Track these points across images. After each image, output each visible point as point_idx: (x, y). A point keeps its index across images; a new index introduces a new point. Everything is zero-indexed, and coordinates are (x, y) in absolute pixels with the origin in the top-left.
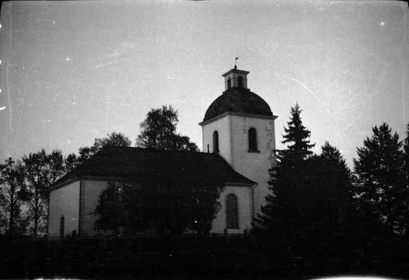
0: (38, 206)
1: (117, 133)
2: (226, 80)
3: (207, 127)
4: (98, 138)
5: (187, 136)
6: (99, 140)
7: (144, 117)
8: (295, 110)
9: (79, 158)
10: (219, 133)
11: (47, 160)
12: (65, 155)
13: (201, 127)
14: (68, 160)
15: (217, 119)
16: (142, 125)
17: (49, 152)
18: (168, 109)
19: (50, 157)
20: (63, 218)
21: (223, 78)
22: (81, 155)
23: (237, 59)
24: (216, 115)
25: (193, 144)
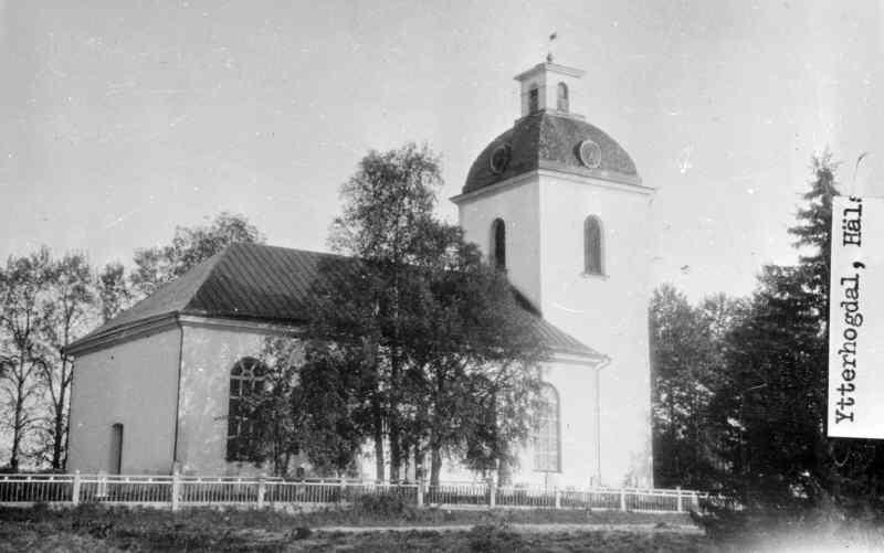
0: (25, 392)
1: (233, 214)
2: (526, 91)
3: (471, 208)
4: (183, 225)
5: (584, 219)
6: (186, 229)
7: (353, 169)
8: (820, 161)
9: (804, 282)
10: (508, 230)
11: (50, 276)
12: (98, 266)
13: (456, 207)
14: (105, 279)
15: (495, 192)
16: (346, 190)
17: (57, 257)
18: (419, 151)
19: (61, 269)
20: (119, 428)
21: (518, 84)
22: (138, 267)
23: (553, 37)
24: (498, 178)
25: (473, 247)
